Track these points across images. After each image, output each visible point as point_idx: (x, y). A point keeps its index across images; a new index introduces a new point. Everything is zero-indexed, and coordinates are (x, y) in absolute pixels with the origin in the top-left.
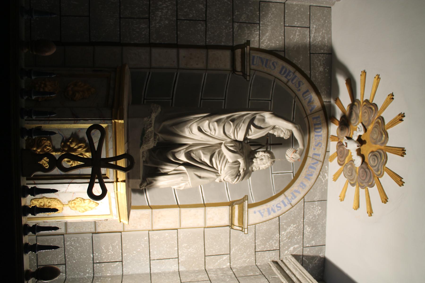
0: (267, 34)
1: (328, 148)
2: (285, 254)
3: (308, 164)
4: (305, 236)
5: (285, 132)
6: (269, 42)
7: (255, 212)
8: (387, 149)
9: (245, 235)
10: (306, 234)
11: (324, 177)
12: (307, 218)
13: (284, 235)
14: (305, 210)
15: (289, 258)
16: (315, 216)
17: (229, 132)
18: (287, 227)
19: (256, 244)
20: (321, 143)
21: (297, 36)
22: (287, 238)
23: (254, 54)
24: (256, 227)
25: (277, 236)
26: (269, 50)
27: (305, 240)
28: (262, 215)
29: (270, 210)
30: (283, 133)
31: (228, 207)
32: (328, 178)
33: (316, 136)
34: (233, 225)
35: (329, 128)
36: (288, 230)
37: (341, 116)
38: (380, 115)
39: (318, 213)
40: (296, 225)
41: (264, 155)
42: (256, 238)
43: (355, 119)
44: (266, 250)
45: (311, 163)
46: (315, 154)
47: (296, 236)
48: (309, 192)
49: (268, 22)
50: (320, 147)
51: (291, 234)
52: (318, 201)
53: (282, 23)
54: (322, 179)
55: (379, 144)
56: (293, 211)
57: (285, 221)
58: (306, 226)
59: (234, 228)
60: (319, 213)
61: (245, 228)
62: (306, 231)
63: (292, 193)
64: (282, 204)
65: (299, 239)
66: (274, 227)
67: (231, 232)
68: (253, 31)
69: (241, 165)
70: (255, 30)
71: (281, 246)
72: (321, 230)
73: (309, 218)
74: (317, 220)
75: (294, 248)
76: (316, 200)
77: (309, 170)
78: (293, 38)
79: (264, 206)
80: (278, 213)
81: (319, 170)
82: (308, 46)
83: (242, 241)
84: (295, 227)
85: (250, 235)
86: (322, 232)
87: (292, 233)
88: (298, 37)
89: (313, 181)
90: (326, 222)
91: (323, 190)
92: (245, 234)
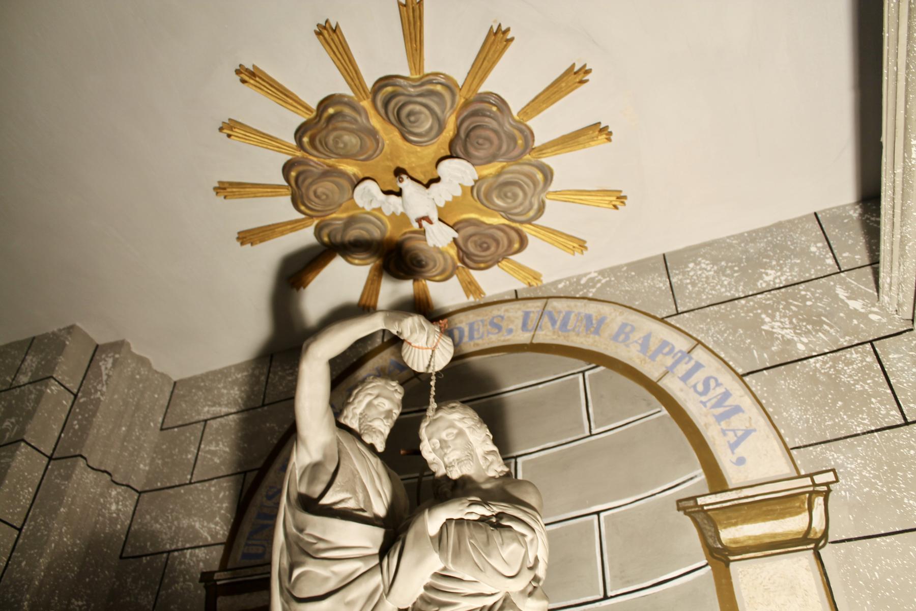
0: (197, 525)
1: (507, 297)
2: (884, 320)
3: (555, 337)
4: (796, 280)
5: (370, 394)
6: (217, 519)
7: (741, 461)
8: (355, 85)
9: (842, 481)
10: (790, 278)
11: (592, 282)
12: (729, 291)
13: (810, 342)
14: (703, 304)
15: (890, 297)
16: (721, 271)
17: (326, 579)
18: (777, 339)
19: (873, 428)
20: (494, 318)
21: (218, 448)
22: (817, 331)
23: (237, 558)
24: (797, 445)
25: (818, 365)
26: (234, 515)
27: (811, 275)
28: (748, 432)
29: (720, 410)
30: (376, 402)
31: (732, 565)
32: (595, 272)
33: (471, 337)
34: (811, 536)
35: (451, 310)
36: (789, 334)
37: (398, 280)
38: (295, 147)
39: (707, 264)
40: (763, 316)
41: (429, 440)
42: (843, 433)
43: (361, 225)
44: (886, 385)
45: (551, 328)
46: (524, 327)
47: (805, 306)
48: (644, 310)
49: (170, 528)
50: (502, 318)
51: (799, 320)
52: (669, 277)
53: (182, 491)
54: (599, 285)
55: (365, 121)
56: (712, 336)
57: (755, 352)
58: (761, 285)
59: (823, 527)
60: (708, 262)
61: (814, 485)
62: (777, 281)
63: (653, 357)
64: (692, 381)
65: (813, 293)
66: (784, 381)
67: (844, 537)
68: (183, 567)
69: (457, 516)
70: (181, 563)
71: (856, 342)
72: (765, 240)
73: (729, 284)
74: (732, 263)
75: (849, 298)
76: (668, 284)
77: (573, 330)
78: (219, 458)
79: (713, 435)
80: (729, 382)
81: (572, 303)
82: (245, 415)
83: (873, 486)
84: (773, 317)
85: (838, 458)
86: (772, 236)
87: (794, 320)
88: (221, 443)
89: (606, 309)
90: (733, 236)
91: (633, 273)
92: (837, 481)
